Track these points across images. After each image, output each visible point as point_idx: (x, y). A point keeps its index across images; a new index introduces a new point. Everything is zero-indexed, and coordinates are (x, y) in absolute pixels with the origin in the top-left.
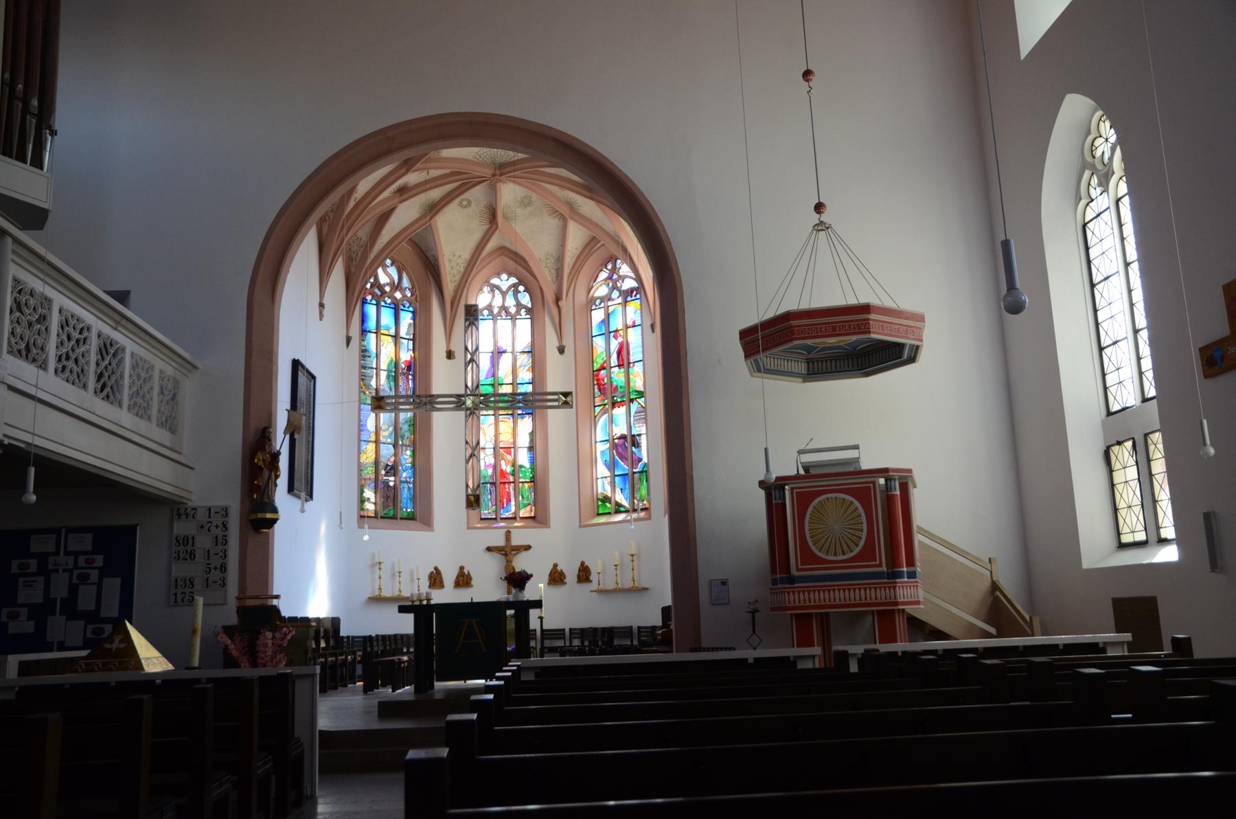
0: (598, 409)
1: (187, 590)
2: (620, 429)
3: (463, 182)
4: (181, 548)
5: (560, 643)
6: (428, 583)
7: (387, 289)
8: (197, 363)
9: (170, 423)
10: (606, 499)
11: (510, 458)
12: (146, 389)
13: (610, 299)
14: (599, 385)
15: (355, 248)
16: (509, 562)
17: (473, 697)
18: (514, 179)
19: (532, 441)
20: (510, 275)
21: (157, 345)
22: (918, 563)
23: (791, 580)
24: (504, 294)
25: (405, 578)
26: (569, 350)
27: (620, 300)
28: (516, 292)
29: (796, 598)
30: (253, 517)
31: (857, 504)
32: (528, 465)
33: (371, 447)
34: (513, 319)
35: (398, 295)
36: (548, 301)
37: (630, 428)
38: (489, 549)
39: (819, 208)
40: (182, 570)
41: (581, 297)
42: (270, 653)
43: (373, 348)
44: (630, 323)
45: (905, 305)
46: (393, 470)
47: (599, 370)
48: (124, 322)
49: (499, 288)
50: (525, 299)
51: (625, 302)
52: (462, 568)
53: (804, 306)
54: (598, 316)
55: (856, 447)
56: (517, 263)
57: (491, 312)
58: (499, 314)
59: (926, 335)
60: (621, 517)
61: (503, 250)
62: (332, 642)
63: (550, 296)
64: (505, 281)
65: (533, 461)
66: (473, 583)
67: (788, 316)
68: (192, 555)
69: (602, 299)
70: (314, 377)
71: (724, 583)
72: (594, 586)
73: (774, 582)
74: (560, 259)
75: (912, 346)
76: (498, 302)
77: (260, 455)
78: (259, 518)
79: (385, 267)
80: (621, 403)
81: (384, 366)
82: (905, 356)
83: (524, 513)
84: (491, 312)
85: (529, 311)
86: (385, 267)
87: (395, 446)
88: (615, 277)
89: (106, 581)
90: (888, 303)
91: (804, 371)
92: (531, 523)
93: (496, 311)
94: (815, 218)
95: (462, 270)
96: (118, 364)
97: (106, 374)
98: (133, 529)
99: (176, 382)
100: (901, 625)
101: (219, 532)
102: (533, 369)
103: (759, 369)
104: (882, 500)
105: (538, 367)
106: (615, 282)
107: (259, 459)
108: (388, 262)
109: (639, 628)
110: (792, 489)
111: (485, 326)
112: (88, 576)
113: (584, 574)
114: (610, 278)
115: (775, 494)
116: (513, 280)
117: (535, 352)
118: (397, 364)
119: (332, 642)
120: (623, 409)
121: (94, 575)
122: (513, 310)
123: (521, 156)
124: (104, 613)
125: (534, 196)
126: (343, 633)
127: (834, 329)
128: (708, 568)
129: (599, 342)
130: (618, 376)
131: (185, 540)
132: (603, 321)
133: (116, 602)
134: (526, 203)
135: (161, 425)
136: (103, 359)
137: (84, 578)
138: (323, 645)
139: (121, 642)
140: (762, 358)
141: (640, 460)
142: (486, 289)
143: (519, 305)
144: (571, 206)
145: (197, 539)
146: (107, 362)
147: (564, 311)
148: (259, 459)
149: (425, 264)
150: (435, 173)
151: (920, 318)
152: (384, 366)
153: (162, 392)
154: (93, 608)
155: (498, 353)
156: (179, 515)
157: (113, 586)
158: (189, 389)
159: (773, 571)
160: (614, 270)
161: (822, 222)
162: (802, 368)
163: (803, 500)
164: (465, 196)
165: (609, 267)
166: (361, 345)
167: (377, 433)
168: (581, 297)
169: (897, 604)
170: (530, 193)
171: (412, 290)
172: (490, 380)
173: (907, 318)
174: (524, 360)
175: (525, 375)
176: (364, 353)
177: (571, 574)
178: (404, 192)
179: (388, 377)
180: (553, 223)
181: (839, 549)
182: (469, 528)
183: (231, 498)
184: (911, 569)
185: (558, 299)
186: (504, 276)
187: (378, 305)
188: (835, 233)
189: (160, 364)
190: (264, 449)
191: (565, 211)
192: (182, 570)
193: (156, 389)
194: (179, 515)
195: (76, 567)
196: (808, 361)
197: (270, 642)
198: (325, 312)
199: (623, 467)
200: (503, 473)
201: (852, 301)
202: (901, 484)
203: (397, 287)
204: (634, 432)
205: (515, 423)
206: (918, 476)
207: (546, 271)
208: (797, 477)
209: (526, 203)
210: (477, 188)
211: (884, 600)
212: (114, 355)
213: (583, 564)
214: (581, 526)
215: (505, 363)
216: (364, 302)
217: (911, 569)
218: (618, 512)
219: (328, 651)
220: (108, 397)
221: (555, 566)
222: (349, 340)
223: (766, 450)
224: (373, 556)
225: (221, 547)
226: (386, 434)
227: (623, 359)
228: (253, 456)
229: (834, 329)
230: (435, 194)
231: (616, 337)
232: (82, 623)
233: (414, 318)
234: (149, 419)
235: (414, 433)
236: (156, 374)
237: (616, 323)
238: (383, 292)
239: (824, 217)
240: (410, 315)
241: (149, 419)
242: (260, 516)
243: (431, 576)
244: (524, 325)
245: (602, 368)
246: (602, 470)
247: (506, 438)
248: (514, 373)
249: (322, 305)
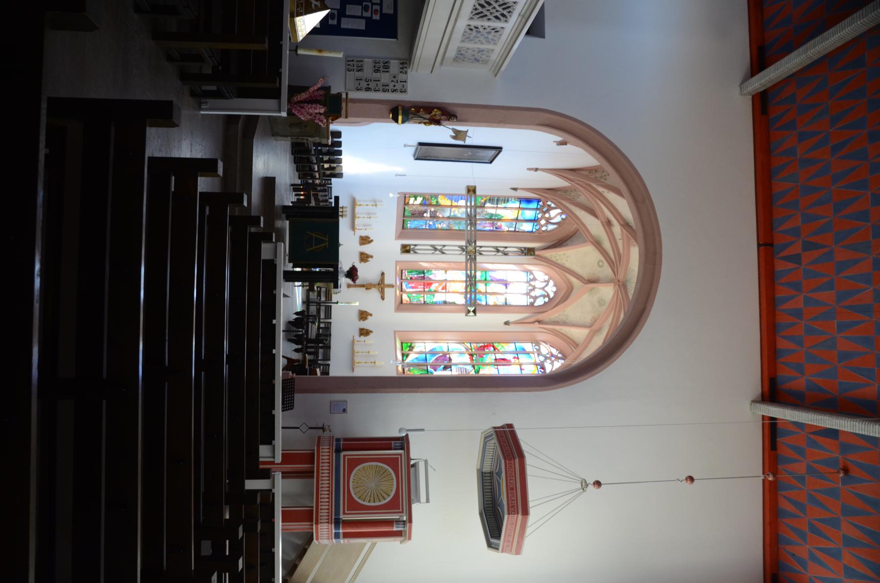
0: (468, 345)
1: (355, 68)
2: (455, 359)
3: (615, 262)
4: (382, 65)
5: (322, 315)
6: (363, 235)
7: (547, 215)
8: (499, 75)
9: (460, 57)
10: (411, 348)
11: (440, 289)
12: (482, 39)
13: (539, 355)
14: (484, 346)
15: (573, 194)
16: (374, 286)
17: (245, 197)
18: (616, 294)
19: (451, 304)
20: (555, 293)
21: (509, 47)
22: (346, 540)
23: (338, 451)
24: (543, 289)
25: (367, 221)
26: (507, 328)
27: (538, 362)
28: (544, 296)
29: (325, 454)
30: (400, 108)
31: (388, 499)
32: (435, 300)
33: (448, 203)
34: (528, 294)
35: (543, 222)
36: (538, 316)
37: (456, 365)
38: (383, 274)
39: (598, 484)
40: (368, 64)
41: (540, 337)
42: (310, 111)
43: (509, 205)
44: (523, 367)
45: (528, 542)
46: (434, 216)
48: (524, 20)
49: (547, 285)
50: (540, 302)
52: (372, 257)
53: (529, 470)
54: (528, 347)
55: (428, 501)
56: (563, 296)
57: (531, 280)
58: (530, 285)
59: (505, 554)
60: (400, 357)
61: (570, 289)
62: (328, 172)
63: (540, 317)
64: (551, 289)
65: (436, 304)
67: (521, 456)
68: (377, 71)
69: (539, 350)
70: (491, 162)
71: (344, 410)
72: (357, 338)
73: (338, 440)
74: (565, 324)
75: (498, 545)
77: (439, 113)
78: (401, 112)
79: (561, 214)
80: (472, 359)
81: (499, 212)
82: (492, 540)
83: (405, 297)
84: (531, 280)
85: (532, 304)
86: (561, 214)
87: (449, 218)
88: (553, 359)
89: (363, 21)
90: (528, 531)
91: (484, 470)
92: (399, 301)
93: (532, 283)
94: (590, 481)
95: (559, 262)
96: (496, 17)
97: (490, 8)
98: (395, 36)
99: (486, 62)
100: (300, 527)
101: (391, 87)
102: (495, 306)
103: (487, 438)
104: (390, 517)
105: (496, 308)
106: (549, 358)
107: (436, 112)
108: (564, 216)
109: (329, 365)
110: (401, 455)
112: (367, 11)
113: (364, 332)
114: (552, 355)
115: (398, 443)
116: (552, 295)
117: (505, 307)
118: (499, 220)
119: (328, 172)
120: (469, 361)
121: (367, 14)
122: (533, 294)
123: (631, 297)
124: (343, 19)
125: (605, 307)
126: (333, 179)
127: (512, 489)
128: (356, 401)
129: (511, 347)
130: (489, 358)
131: (386, 66)
132: (524, 350)
133: (350, 27)
134: (601, 302)
135: (459, 50)
136: (500, 6)
137: (366, 9)
138: (326, 166)
139: (316, 6)
140: (494, 441)
142: (546, 278)
143: (535, 298)
144: (599, 330)
145: (387, 74)
146: (498, 8)
147: (531, 325)
148: (436, 112)
149: (562, 240)
150: (620, 244)
151: (518, 552)
152: (499, 212)
153: (481, 51)
154: (347, 13)
155: (506, 284)
156: (402, 64)
157: (361, 25)
158: (482, 71)
159: (345, 440)
160: (557, 358)
161: (587, 485)
162: (487, 469)
163: (393, 463)
164: (606, 264)
165: (560, 355)
166: (512, 197)
167: (456, 206)
168: (540, 337)
169: (317, 523)
170: (607, 305)
171: (546, 231)
172: (488, 279)
173: (518, 543)
174: (500, 301)
175: (491, 300)
176: (506, 200)
177: (365, 324)
178: (609, 223)
179: (492, 215)
180: (588, 319)
181: (359, 489)
182: (397, 262)
183: (413, 94)
184: (341, 536)
185: (539, 322)
186: (554, 289)
187: (537, 209)
188: (581, 493)
189: (497, 49)
190: (443, 115)
191: (595, 327)
192: (368, 64)
193: (482, 47)
194: (402, 64)
195: (373, 4)
196: (491, 473)
197: (317, 111)
198: (532, 172)
199: (431, 359)
200: (430, 284)
201: (531, 504)
202: (401, 532)
203: (548, 222)
204: (453, 367)
205: (461, 293)
206: (408, 544)
207: (557, 315)
208: (409, 459)
209: (601, 302)
210: (610, 271)
211: (320, 514)
212: (503, 15)
213: (371, 332)
214: (395, 332)
215: (499, 288)
216: (539, 201)
217: (341, 536)
218: (403, 355)
219: (317, 158)
220: (476, 9)
221: (371, 315)
222: (515, 189)
223: (423, 430)
224: (381, 201)
225: (381, 88)
226: (456, 212)
227: (499, 362)
228: (439, 109)
229: (512, 489)
230: (607, 245)
231: (514, 358)
232: (338, 7)
233: (528, 232)
234: (463, 41)
236: (491, 47)
237: (523, 358)
238: (545, 213)
239: (591, 487)
240: (530, 230)
241: (463, 41)
242: (400, 112)
243: (367, 237)
244: (524, 301)
245: (495, 349)
246: (430, 346)
247: (451, 287)
248: (491, 294)
249: (536, 170)
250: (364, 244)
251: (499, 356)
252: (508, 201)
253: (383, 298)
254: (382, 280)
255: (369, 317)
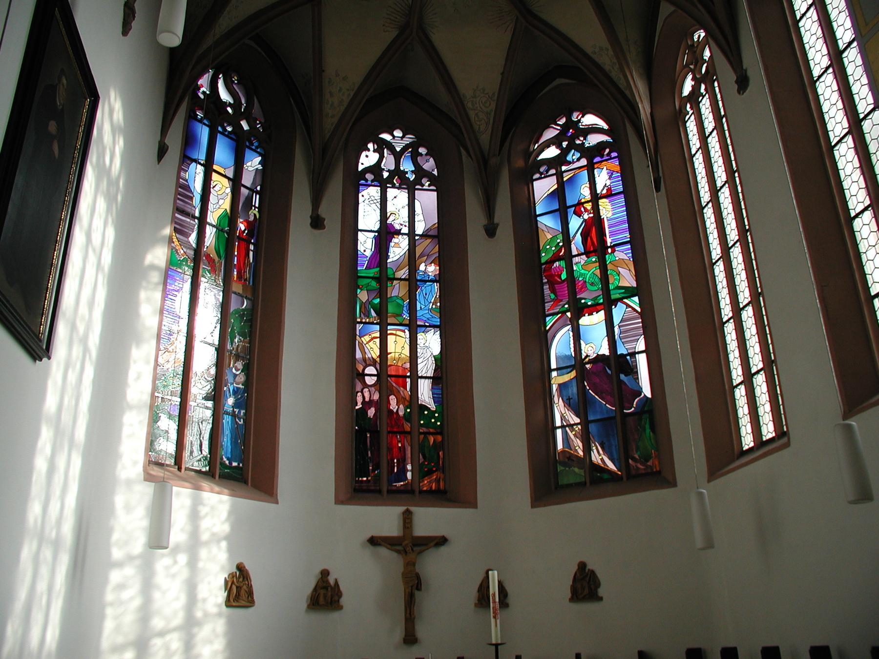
24: (398, 156)
38: (374, 541)
47: (551, 262)
50: (429, 165)
51: (590, 168)
52: (325, 573)
54: (543, 187)
64: (398, 138)
66: (343, 601)
76: (389, 163)
85: (433, 180)
111: (369, 195)
116: (409, 139)
129: (548, 223)
130: (585, 268)
141: (639, 392)
143: (420, 172)
152: (213, 217)
186: (398, 133)
204: (621, 350)
213: (582, 566)
215: (398, 249)
216: (191, 117)
235: (251, 334)
243: (229, 585)
244: (428, 200)
245: (556, 258)
250: (250, 593)
251: (577, 244)
252: (187, 188)
253: (441, 541)
254: (389, 542)
255: (590, 566)
